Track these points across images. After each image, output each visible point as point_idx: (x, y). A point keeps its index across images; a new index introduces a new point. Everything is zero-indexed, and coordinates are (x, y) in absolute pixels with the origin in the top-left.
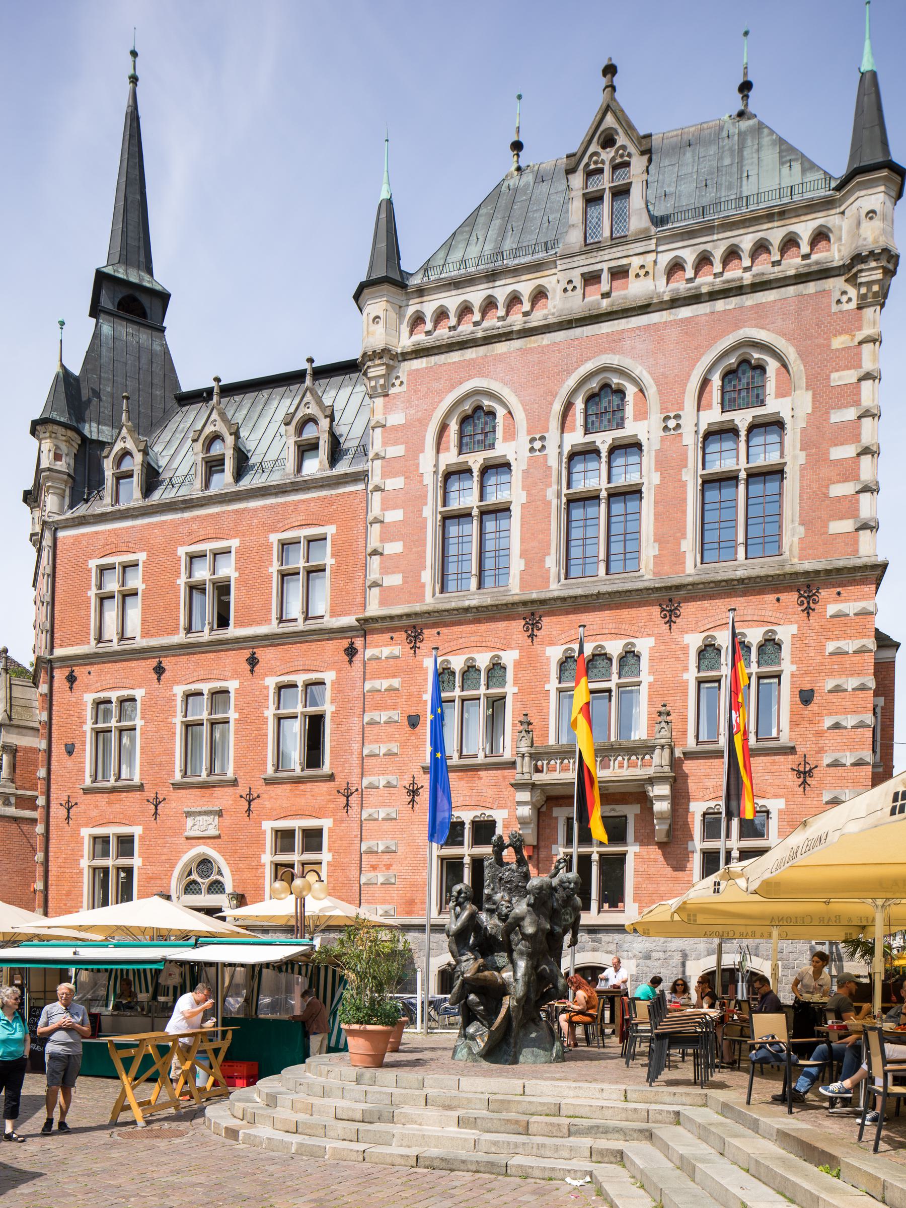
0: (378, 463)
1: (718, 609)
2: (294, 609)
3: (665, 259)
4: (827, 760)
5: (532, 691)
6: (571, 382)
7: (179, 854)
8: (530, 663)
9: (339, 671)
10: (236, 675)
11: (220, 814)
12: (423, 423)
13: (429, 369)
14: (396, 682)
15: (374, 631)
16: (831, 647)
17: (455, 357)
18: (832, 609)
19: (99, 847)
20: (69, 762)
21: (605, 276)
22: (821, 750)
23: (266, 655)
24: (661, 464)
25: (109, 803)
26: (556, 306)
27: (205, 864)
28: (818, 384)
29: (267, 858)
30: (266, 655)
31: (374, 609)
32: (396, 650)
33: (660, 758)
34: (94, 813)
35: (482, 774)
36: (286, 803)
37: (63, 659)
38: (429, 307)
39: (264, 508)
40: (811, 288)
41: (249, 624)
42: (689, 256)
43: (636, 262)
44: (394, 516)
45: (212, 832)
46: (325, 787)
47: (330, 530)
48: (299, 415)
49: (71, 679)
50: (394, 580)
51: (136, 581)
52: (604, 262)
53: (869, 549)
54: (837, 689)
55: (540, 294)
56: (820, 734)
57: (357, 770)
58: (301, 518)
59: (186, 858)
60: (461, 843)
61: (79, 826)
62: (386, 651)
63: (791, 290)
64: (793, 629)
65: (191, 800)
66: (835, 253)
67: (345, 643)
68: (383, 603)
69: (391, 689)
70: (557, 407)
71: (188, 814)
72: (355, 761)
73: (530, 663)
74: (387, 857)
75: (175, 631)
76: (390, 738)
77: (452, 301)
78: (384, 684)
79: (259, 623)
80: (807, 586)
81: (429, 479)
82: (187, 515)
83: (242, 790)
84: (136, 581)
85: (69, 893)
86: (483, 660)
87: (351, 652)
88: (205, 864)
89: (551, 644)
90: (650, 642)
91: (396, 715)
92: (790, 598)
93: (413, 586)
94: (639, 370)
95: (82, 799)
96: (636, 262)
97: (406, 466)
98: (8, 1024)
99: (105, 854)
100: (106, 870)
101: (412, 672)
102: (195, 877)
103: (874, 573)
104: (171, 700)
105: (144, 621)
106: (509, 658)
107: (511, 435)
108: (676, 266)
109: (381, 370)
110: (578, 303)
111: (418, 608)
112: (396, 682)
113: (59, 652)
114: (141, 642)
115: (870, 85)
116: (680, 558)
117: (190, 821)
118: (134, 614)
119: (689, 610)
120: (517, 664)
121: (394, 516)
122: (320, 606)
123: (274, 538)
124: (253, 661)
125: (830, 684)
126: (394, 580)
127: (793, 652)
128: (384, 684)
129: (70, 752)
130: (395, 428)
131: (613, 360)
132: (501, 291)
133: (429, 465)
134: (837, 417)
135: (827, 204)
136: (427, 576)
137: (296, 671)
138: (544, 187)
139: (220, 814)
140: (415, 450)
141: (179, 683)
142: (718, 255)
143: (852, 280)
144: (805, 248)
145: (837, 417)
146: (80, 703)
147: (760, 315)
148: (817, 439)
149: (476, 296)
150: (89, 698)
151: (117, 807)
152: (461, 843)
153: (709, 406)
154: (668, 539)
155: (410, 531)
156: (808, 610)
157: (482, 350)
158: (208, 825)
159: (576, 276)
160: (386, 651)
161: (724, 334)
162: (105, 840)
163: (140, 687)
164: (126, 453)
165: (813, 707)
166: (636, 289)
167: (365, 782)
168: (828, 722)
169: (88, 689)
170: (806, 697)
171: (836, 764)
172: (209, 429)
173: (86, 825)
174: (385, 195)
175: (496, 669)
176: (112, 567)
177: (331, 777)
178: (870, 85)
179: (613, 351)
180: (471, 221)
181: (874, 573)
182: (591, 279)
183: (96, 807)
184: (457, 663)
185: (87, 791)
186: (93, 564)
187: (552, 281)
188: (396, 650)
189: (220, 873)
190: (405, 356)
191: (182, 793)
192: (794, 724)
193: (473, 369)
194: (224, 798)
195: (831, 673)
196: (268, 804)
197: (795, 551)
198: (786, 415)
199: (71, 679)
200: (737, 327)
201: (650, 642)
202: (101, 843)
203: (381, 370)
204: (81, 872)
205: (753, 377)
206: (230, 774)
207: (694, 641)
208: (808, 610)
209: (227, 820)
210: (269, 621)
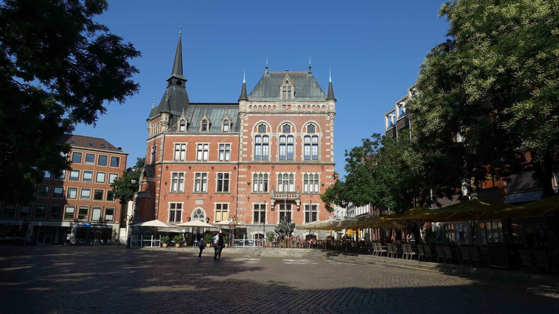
2: (222, 158)
3: (297, 105)
5: (273, 181)
7: (193, 209)
8: (273, 175)
12: (252, 126)
23: (216, 167)
28: (323, 131)
29: (222, 203)
33: (298, 195)
46: (228, 195)
49: (167, 167)
51: (230, 148)
52: (287, 103)
57: (236, 193)
66: (326, 110)
68: (243, 160)
72: (236, 191)
73: (273, 175)
75: (195, 160)
83: (209, 195)
84: (230, 148)
85: (164, 217)
86: (263, 173)
88: (199, 211)
92: (319, 167)
96: (292, 105)
104: (193, 174)
110: (282, 109)
111: (250, 162)
112: (245, 176)
113: (164, 162)
116: (301, 158)
122: (227, 158)
123: (218, 143)
133: (253, 134)
134: (327, 138)
138: (273, 80)
140: (250, 131)
145: (327, 138)
159: (281, 105)
166: (293, 109)
175: (266, 175)
176: (201, 145)
180: (259, 84)
184: (258, 173)
186: (174, 143)
187: (277, 104)
199: (167, 167)
202: (173, 206)
205: (483, 39)
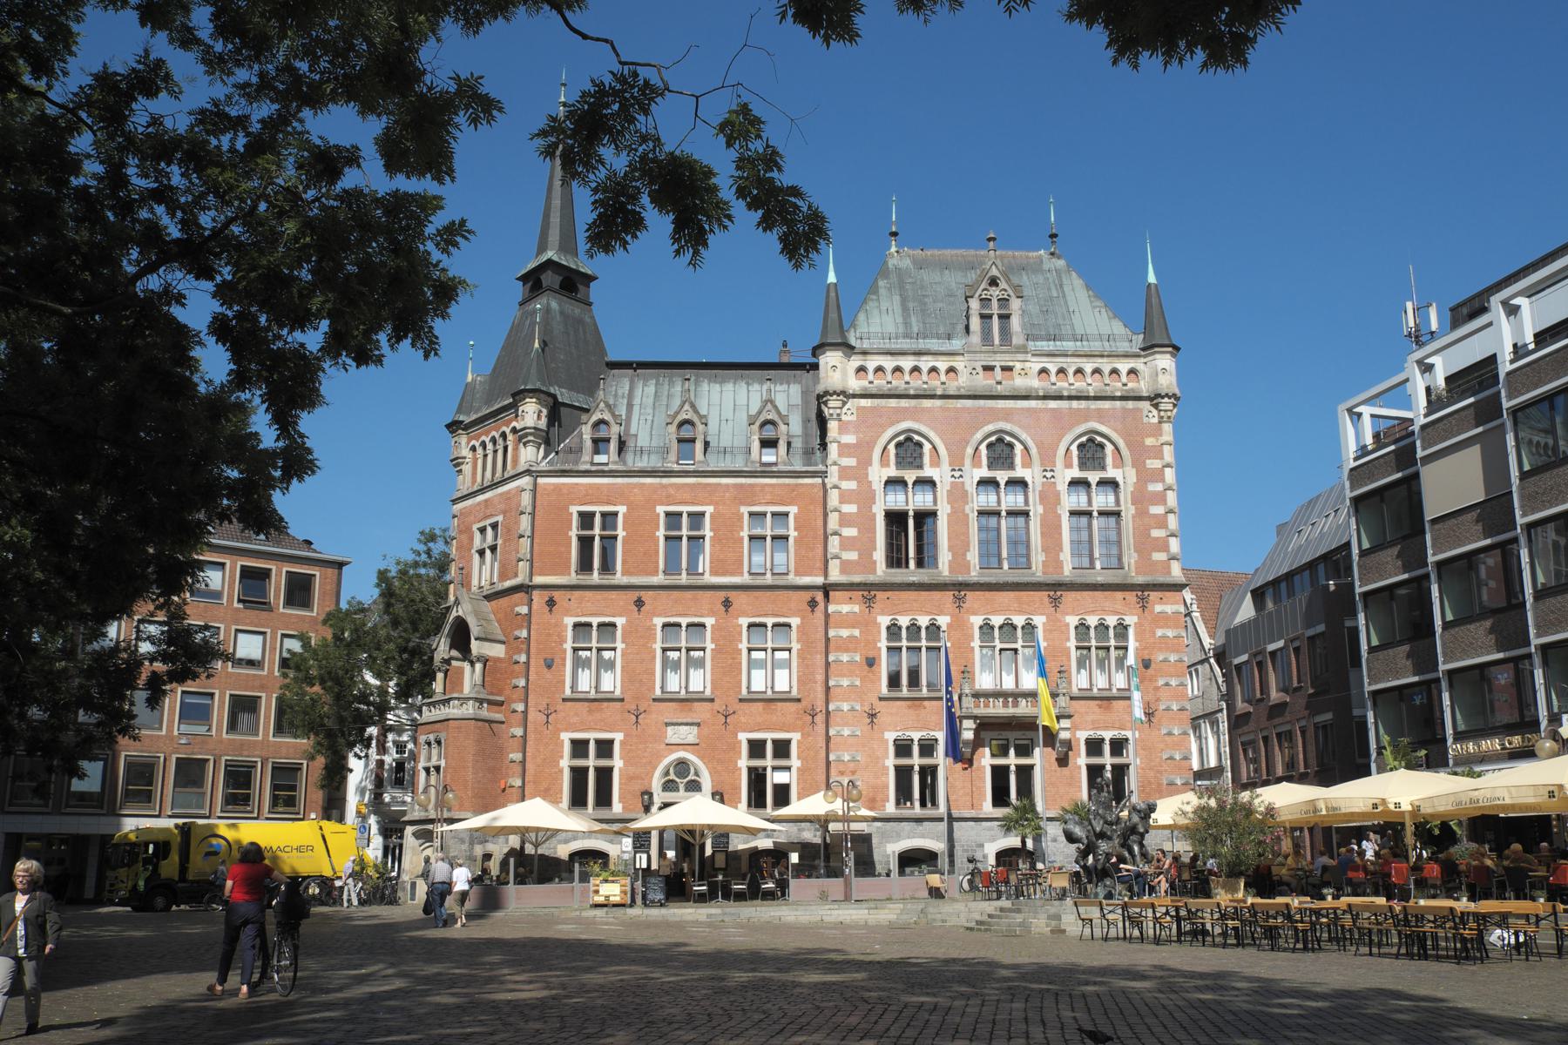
0: (835, 468)
3: (1038, 367)
4: (1162, 707)
6: (979, 435)
7: (660, 758)
9: (803, 618)
10: (711, 613)
11: (698, 725)
12: (870, 445)
13: (873, 409)
14: (856, 633)
16: (1159, 633)
17: (893, 403)
20: (548, 675)
21: (998, 370)
22: (1158, 700)
25: (590, 711)
26: (963, 381)
27: (682, 767)
28: (1138, 464)
30: (739, 599)
31: (835, 575)
32: (856, 608)
34: (575, 720)
35: (926, 703)
36: (759, 720)
38: (872, 363)
39: (735, 485)
40: (1130, 404)
41: (723, 574)
44: (850, 508)
45: (691, 739)
47: (793, 510)
48: (762, 419)
49: (551, 603)
50: (852, 556)
54: (1165, 660)
56: (1157, 689)
58: (768, 497)
59: (666, 761)
60: (1113, 766)
61: (559, 731)
63: (1118, 404)
66: (1143, 387)
68: (843, 571)
69: (851, 637)
70: (970, 451)
71: (667, 724)
73: (959, 625)
74: (852, 765)
75: (655, 573)
76: (851, 674)
77: (889, 363)
79: (732, 574)
82: (665, 481)
86: (923, 621)
88: (682, 767)
89: (975, 614)
93: (867, 563)
95: (561, 706)
96: (1018, 366)
97: (859, 473)
101: (868, 625)
102: (672, 776)
107: (936, 461)
109: (839, 404)
112: (856, 633)
116: (1059, 565)
120: (949, 625)
121: (850, 508)
126: (852, 556)
127: (1136, 634)
129: (549, 667)
130: (847, 445)
131: (1008, 427)
132: (925, 363)
133: (879, 474)
136: (880, 555)
137: (766, 615)
139: (698, 725)
140: (865, 463)
141: (659, 615)
143: (1156, 406)
144: (871, 376)
146: (560, 626)
147: (1101, 416)
149: (907, 363)
152: (1113, 766)
153: (888, 465)
154: (959, 550)
157: (913, 402)
158: (688, 734)
159: (978, 366)
161: (1078, 423)
163: (621, 615)
165: (1150, 671)
166: (1019, 383)
168: (1161, 682)
169: (568, 613)
171: (1168, 709)
173: (566, 730)
179: (1006, 420)
183: (576, 714)
188: (856, 608)
189: (697, 774)
190: (854, 396)
191: (569, 704)
193: (1007, 415)
194: (701, 711)
195: (1160, 649)
196: (743, 719)
198: (1120, 480)
199: (551, 603)
200: (1086, 421)
202: (579, 748)
203: (839, 404)
204: (561, 771)
209: (706, 731)
210: (742, 574)
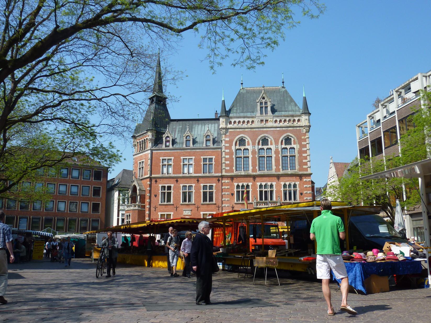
1: (286, 178)
3: (274, 120)
6: (259, 138)
14: (229, 187)
15: (224, 177)
16: (305, 186)
18: (304, 180)
19: (163, 189)
23: (201, 180)
24: (275, 153)
32: (229, 181)
37: (154, 178)
42: (278, 120)
43: (270, 119)
49: (156, 181)
53: (309, 171)
54: (306, 193)
55: (253, 122)
62: (227, 181)
64: (299, 183)
65: (184, 208)
67: (218, 179)
70: (257, 141)
75: (180, 173)
76: (228, 197)
78: (227, 187)
80: (301, 176)
81: (234, 151)
87: (219, 180)
90: (275, 183)
91: (229, 193)
94: (271, 137)
96: (270, 119)
97: (230, 148)
98: (178, 35)
99: (165, 190)
100: (165, 193)
101: (232, 185)
103: (310, 175)
105: (173, 171)
106: (250, 184)
108: (276, 121)
112: (229, 187)
113: (153, 176)
114: (172, 175)
115: (305, 98)
117: (184, 212)
118: (171, 170)
119: (281, 178)
120: (252, 185)
123: (202, 157)
124: (198, 181)
125: (305, 192)
128: (227, 187)
131: (266, 135)
135: (300, 116)
139: (191, 211)
140: (231, 145)
142: (283, 121)
146: (158, 187)
148: (301, 152)
150: (160, 185)
151: (167, 208)
154: (277, 165)
155: (231, 159)
156: (301, 180)
160: (227, 181)
162: (165, 187)
164: (168, 137)
165: (303, 196)
167: (223, 205)
170: (301, 194)
172: (187, 135)
174: (223, 99)
175: (248, 186)
177: (215, 204)
178: (305, 98)
181: (310, 175)
182: (262, 121)
185: (160, 205)
186: (161, 158)
188: (229, 181)
192: (300, 198)
195: (305, 190)
197: (297, 170)
199: (156, 181)
201: (275, 183)
206: (193, 203)
207: (283, 183)
208: (301, 180)
209: (193, 212)
